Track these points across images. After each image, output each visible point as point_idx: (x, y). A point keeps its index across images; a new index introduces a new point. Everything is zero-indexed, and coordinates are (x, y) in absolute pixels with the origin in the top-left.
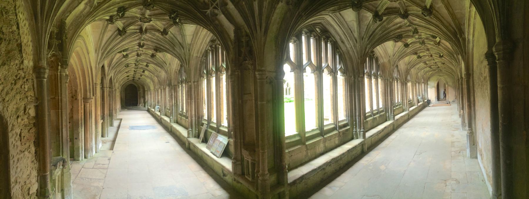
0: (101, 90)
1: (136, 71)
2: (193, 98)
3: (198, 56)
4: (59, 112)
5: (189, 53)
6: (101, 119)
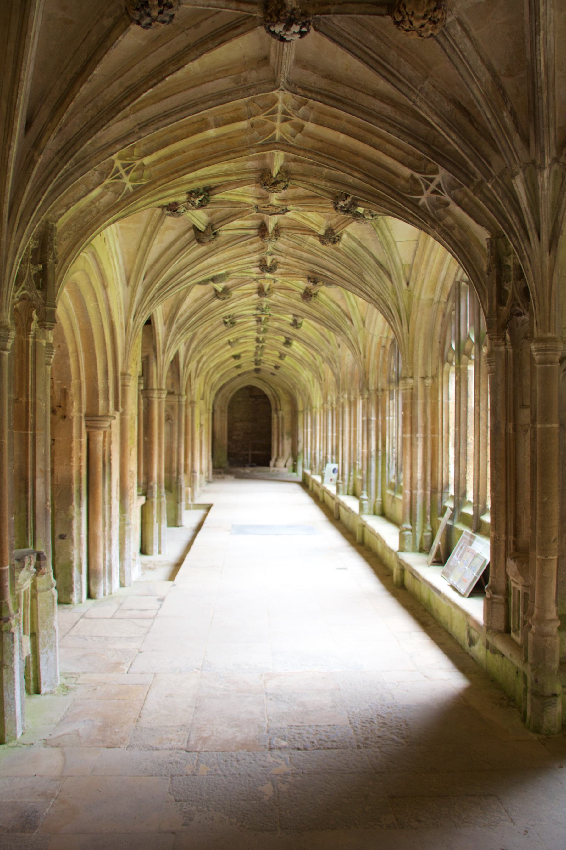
0: (141, 397)
1: (263, 341)
2: (420, 429)
3: (436, 300)
4: (27, 435)
5: (409, 291)
6: (139, 495)
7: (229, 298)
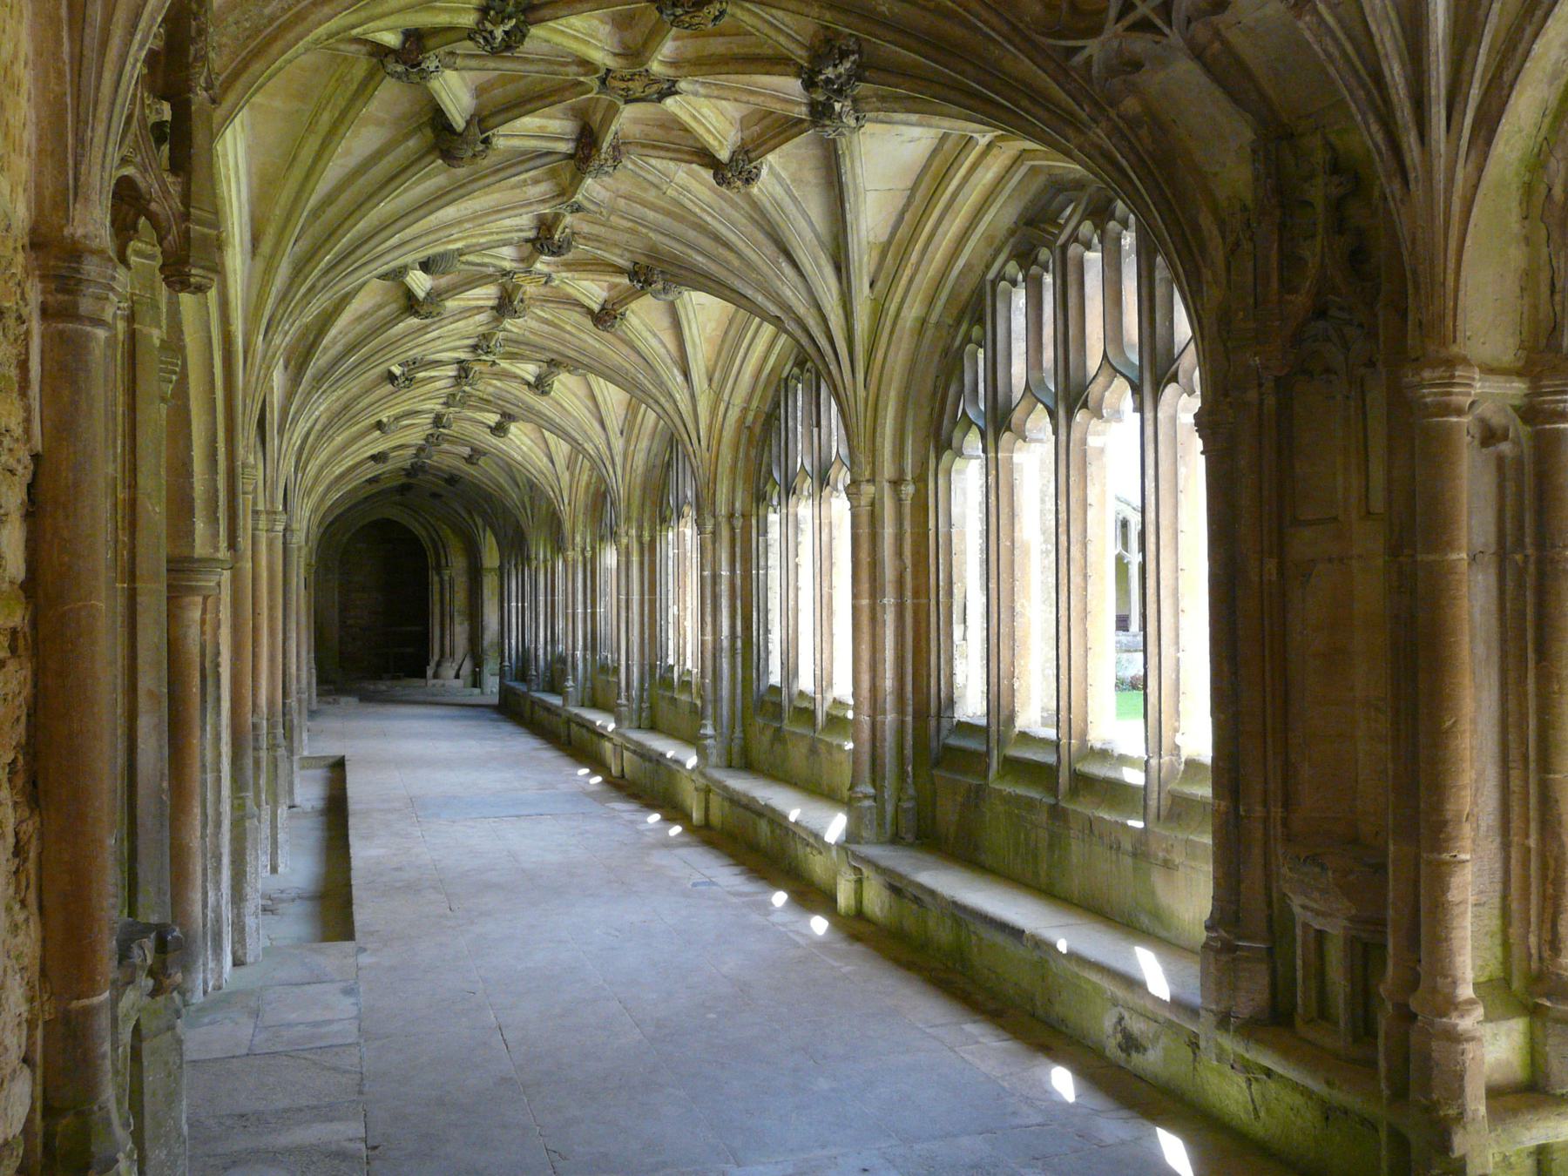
7: (438, 314)
